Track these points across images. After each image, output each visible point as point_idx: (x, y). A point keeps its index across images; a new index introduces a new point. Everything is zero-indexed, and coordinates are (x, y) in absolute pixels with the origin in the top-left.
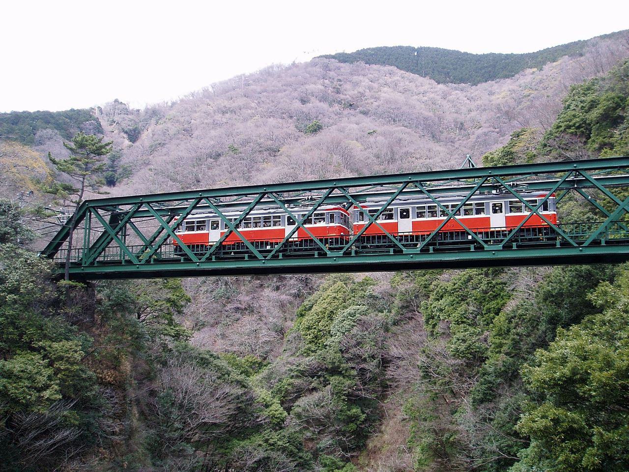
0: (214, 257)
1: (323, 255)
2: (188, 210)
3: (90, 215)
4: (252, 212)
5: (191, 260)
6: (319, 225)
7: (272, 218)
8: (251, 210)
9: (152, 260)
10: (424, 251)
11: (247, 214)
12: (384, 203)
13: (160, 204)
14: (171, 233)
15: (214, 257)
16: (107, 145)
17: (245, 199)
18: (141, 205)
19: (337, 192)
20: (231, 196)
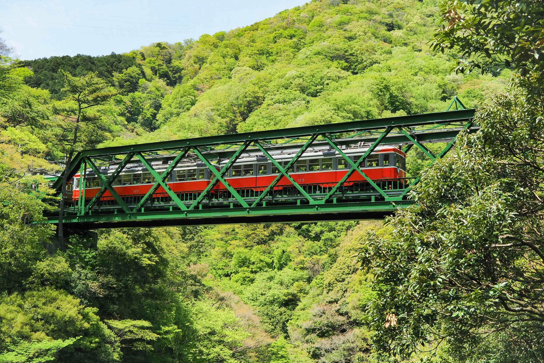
0: (143, 209)
1: (305, 203)
2: (237, 154)
3: (86, 165)
4: (304, 155)
5: (180, 209)
6: (248, 176)
7: (242, 167)
8: (303, 152)
9: (200, 206)
10: (329, 203)
11: (299, 157)
12: (294, 155)
13: (267, 142)
14: (108, 187)
15: (143, 209)
16: (5, 117)
17: (298, 142)
18: (250, 143)
19: (394, 133)
20: (433, 123)
